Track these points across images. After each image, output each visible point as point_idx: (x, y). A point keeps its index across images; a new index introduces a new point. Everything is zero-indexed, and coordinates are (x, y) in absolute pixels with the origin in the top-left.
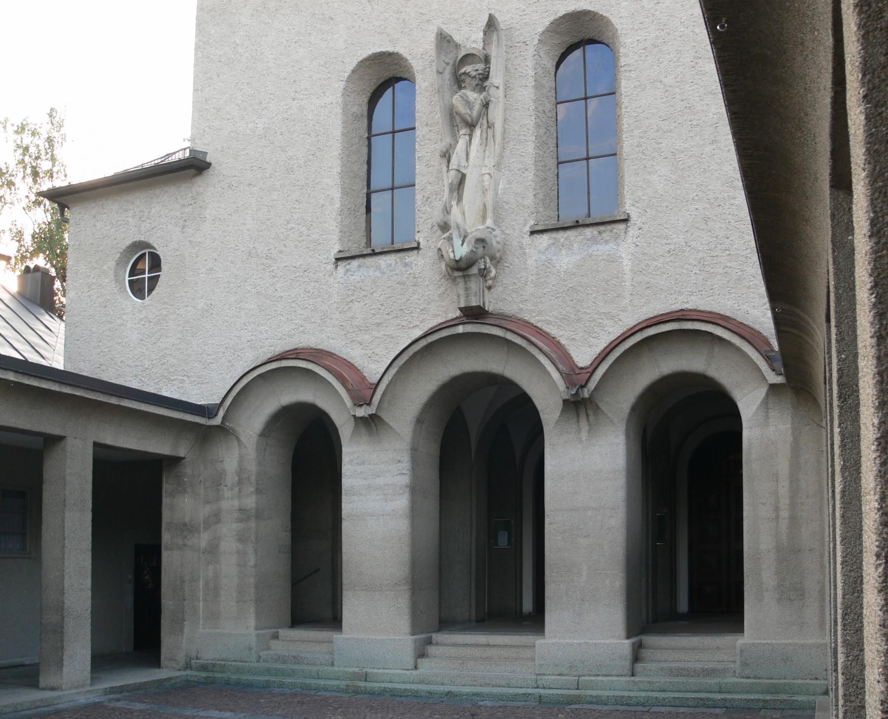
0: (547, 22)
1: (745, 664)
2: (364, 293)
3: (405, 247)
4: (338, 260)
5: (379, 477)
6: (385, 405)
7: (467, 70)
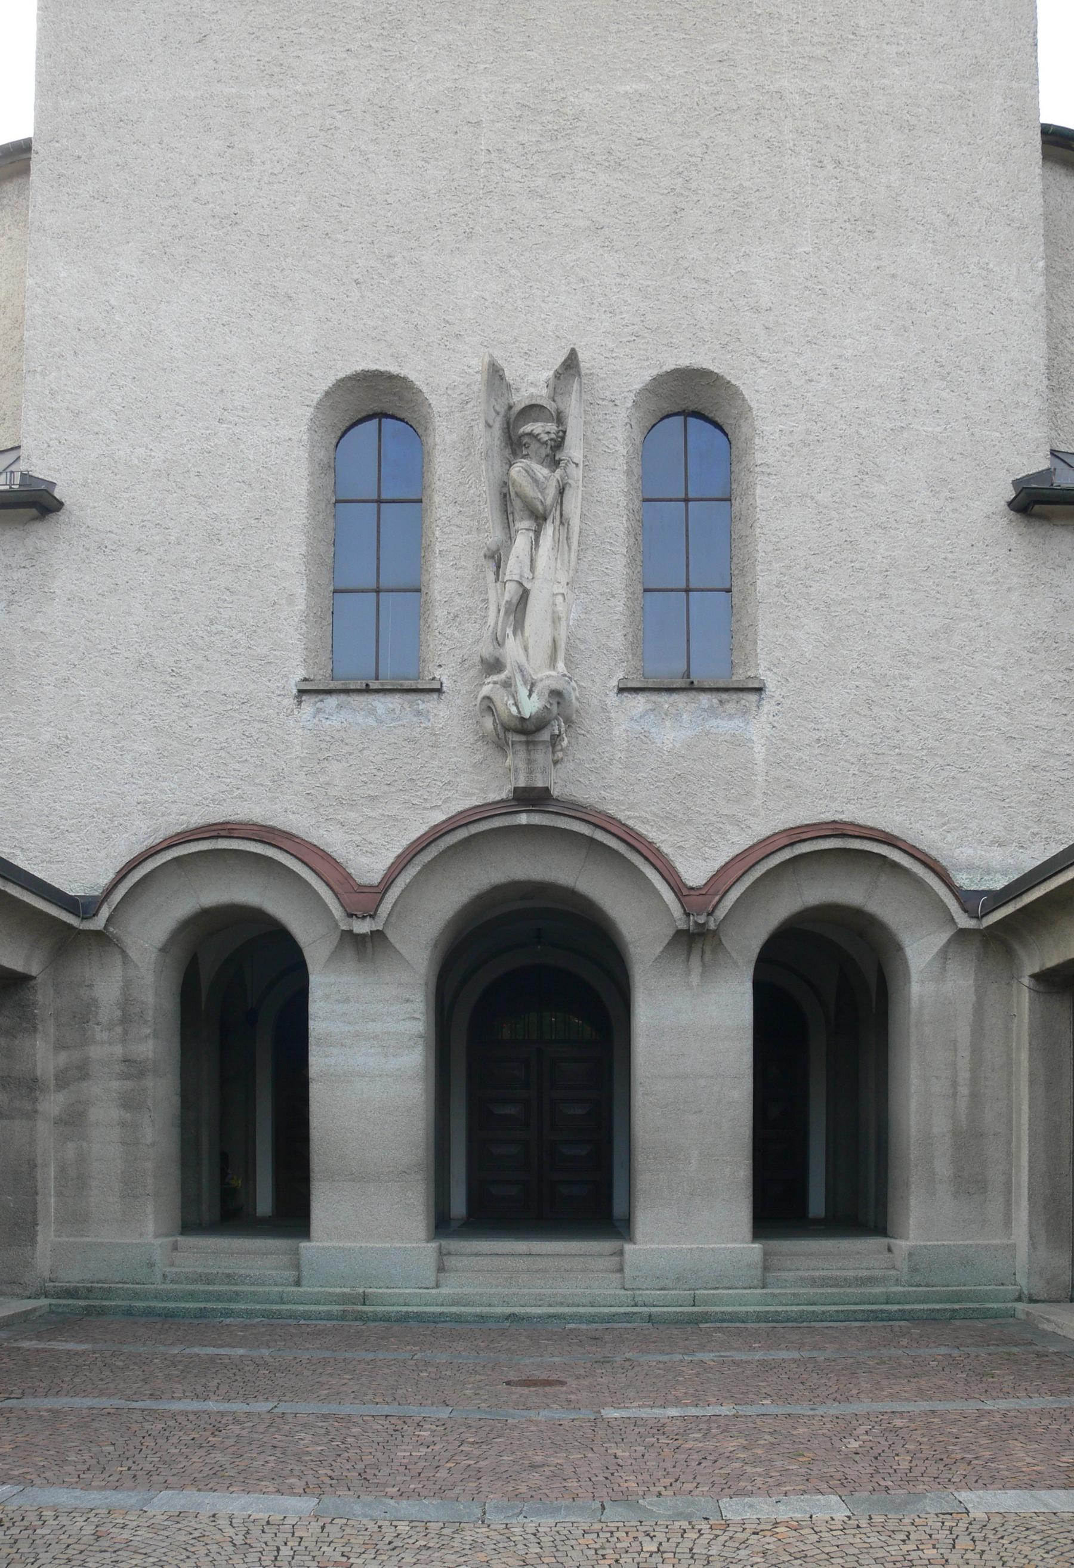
0: (647, 375)
1: (914, 1270)
2: (348, 748)
3: (420, 687)
4: (302, 692)
5: (373, 1021)
6: (393, 919)
7: (526, 431)
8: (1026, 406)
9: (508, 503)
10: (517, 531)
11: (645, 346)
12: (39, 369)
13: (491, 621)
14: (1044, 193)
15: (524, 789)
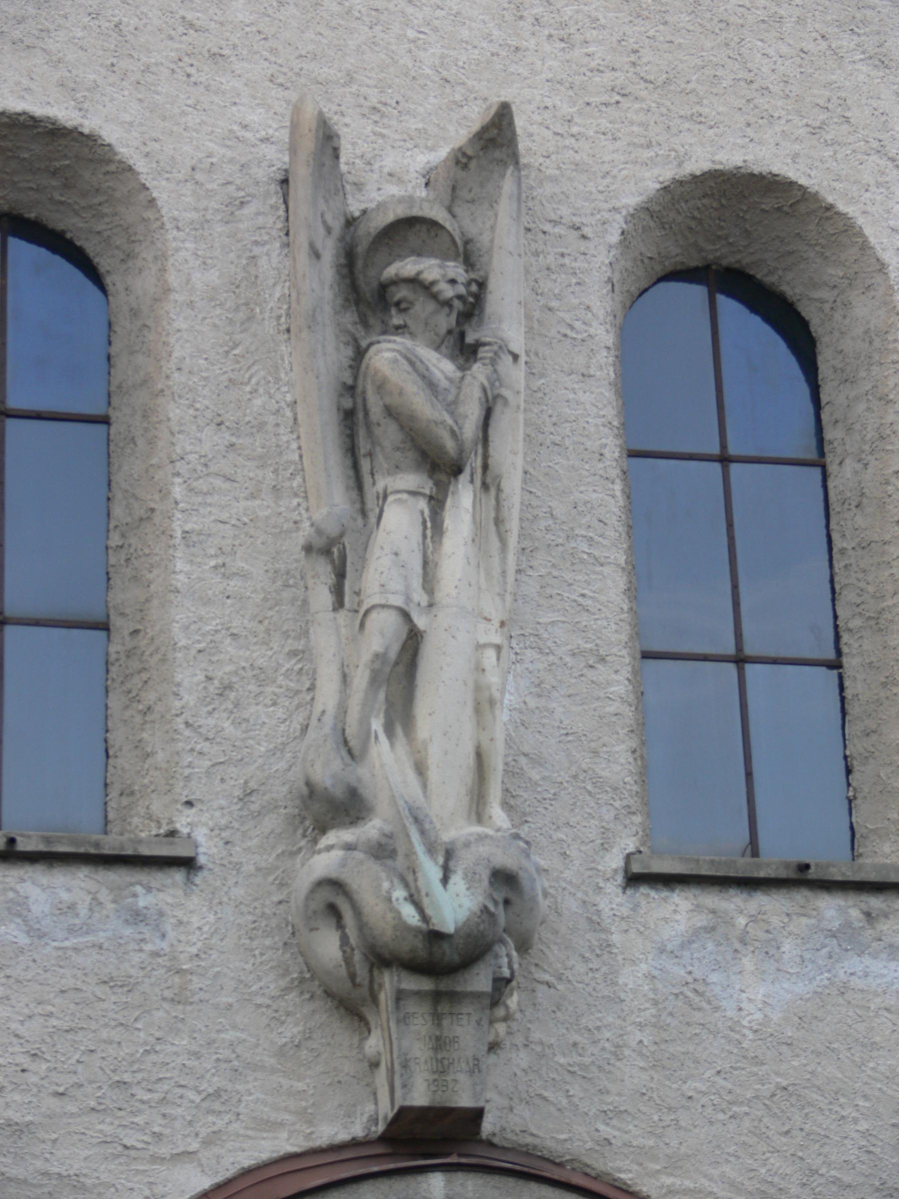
7: (390, 275)
9: (362, 432)
11: (641, 117)
13: (328, 695)
15: (423, 1112)
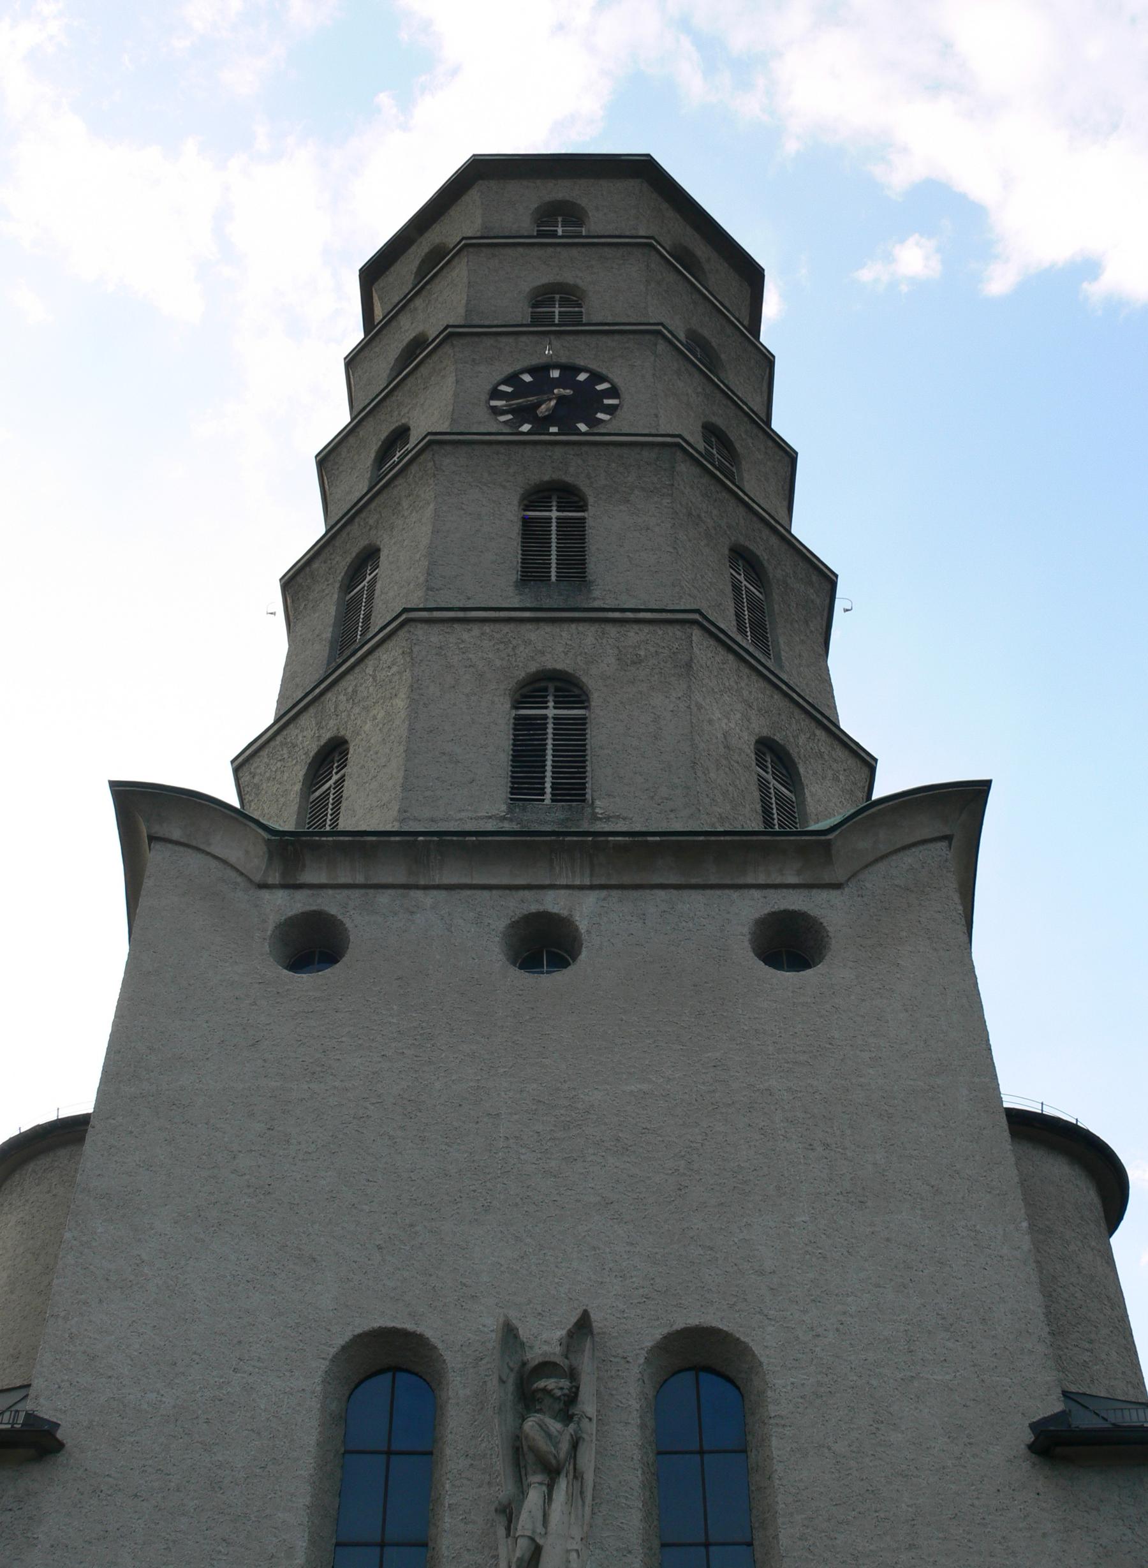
0: (658, 1334)
7: (540, 1387)
8: (1031, 1352)
10: (529, 1485)
12: (62, 1314)
14: (1016, 1164)
